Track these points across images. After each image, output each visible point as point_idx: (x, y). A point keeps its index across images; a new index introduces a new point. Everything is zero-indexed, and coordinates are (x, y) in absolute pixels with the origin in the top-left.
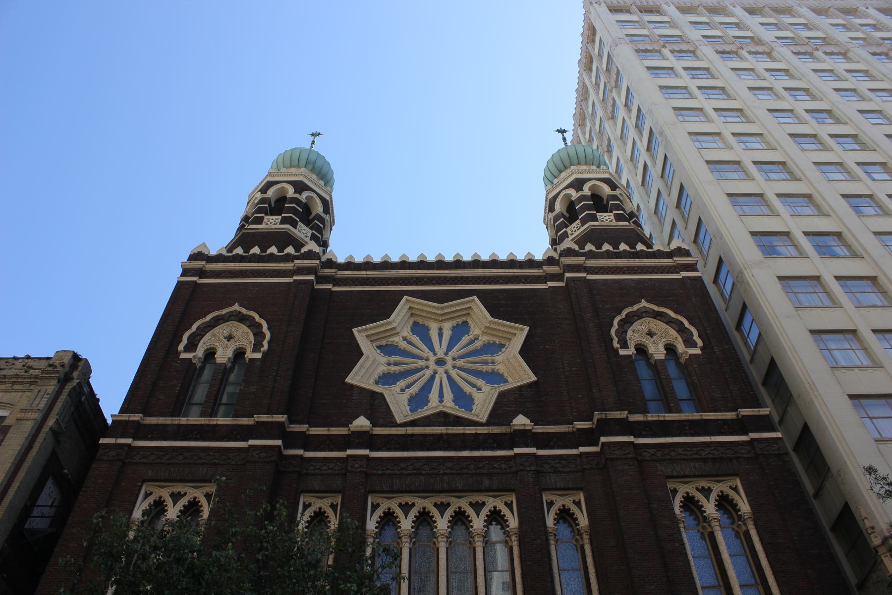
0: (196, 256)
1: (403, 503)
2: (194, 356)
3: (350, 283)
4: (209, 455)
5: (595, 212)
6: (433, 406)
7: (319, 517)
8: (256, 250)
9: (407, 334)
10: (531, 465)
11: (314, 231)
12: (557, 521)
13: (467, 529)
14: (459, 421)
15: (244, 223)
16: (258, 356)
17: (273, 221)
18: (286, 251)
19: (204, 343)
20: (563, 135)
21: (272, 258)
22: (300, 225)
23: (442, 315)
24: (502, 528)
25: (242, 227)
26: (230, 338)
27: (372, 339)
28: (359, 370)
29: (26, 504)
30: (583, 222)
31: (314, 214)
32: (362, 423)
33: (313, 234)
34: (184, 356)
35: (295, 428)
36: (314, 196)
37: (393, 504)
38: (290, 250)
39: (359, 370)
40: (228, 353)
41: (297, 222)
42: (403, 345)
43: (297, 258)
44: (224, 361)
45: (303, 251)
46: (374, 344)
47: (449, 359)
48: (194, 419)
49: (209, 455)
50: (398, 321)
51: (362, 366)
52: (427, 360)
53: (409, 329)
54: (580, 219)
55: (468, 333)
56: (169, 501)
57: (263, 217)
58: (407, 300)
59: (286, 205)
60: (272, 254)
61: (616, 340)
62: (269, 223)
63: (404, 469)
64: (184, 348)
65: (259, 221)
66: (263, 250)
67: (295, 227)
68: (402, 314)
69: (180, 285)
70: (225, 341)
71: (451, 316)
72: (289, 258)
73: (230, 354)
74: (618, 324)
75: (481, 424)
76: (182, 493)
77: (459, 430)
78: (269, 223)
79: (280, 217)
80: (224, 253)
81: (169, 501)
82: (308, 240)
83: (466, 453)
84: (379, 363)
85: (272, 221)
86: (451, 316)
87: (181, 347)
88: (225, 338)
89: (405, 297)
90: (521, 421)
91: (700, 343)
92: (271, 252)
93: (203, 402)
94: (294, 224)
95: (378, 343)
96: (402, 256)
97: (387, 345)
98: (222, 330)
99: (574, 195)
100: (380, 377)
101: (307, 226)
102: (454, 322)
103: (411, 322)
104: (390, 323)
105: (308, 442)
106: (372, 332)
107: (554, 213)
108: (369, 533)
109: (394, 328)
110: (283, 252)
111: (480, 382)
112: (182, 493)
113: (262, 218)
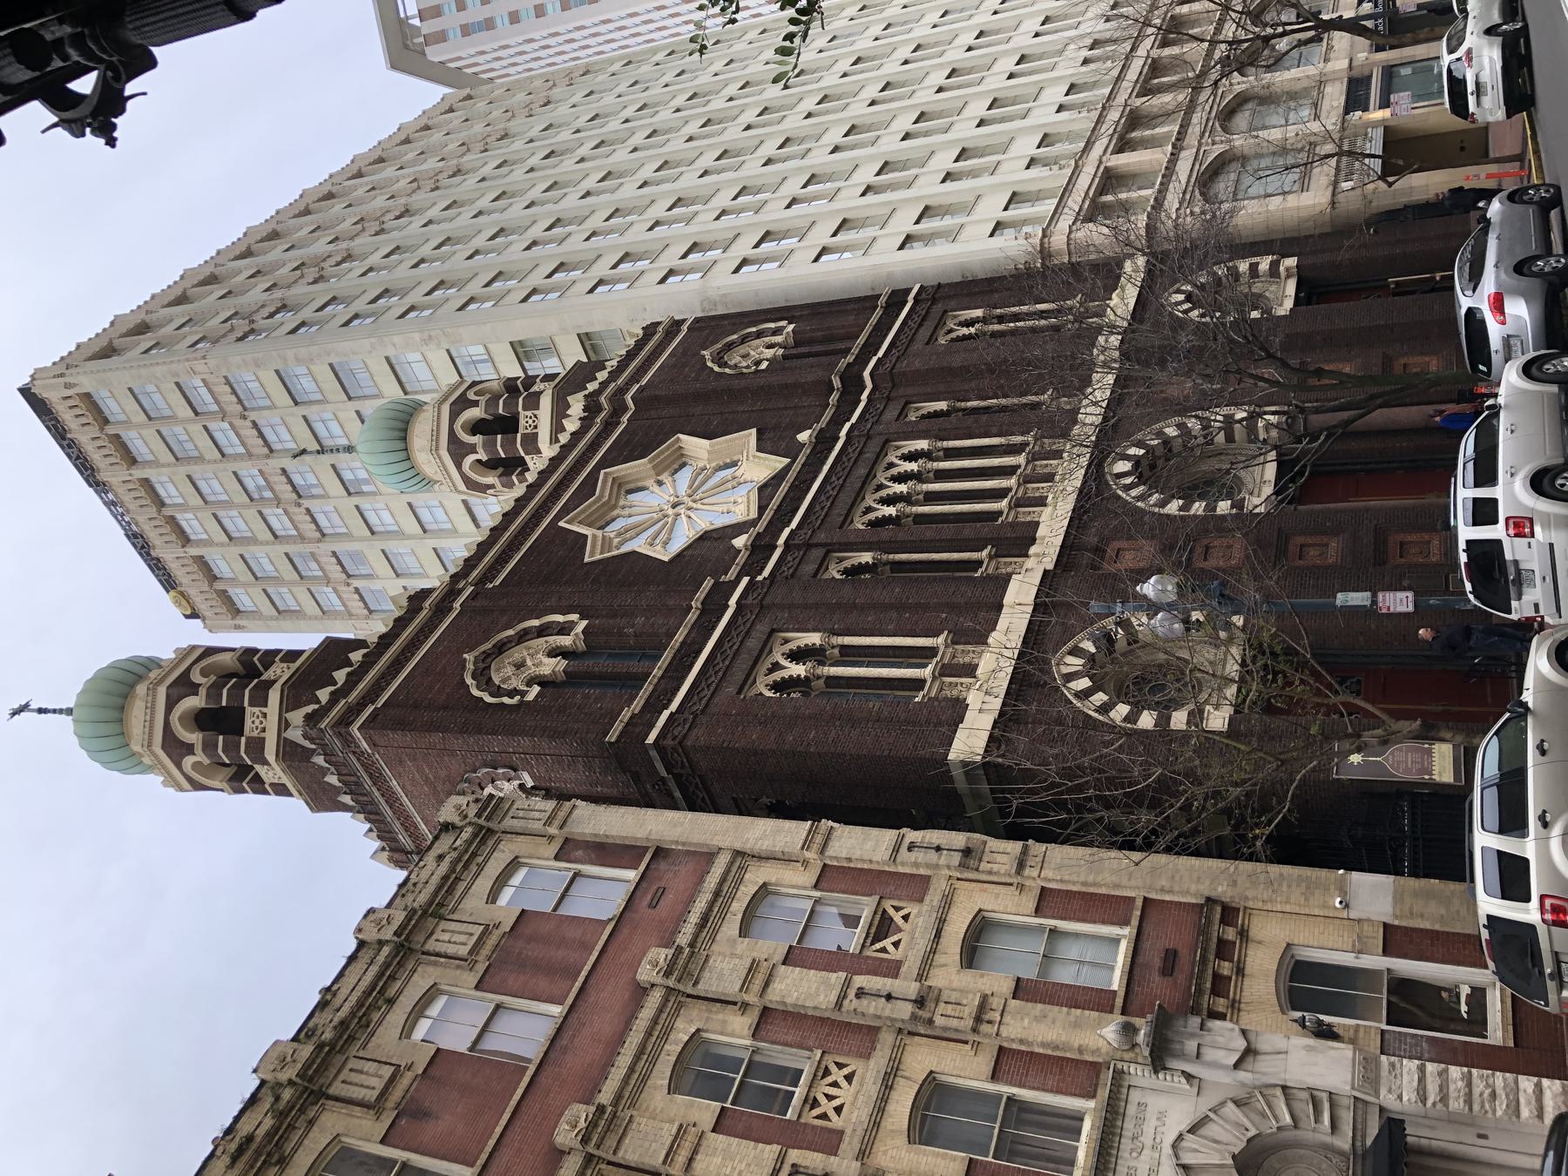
11: (520, 409)
20: (33, 711)
47: (671, 511)
83: (826, 468)
91: (574, 617)
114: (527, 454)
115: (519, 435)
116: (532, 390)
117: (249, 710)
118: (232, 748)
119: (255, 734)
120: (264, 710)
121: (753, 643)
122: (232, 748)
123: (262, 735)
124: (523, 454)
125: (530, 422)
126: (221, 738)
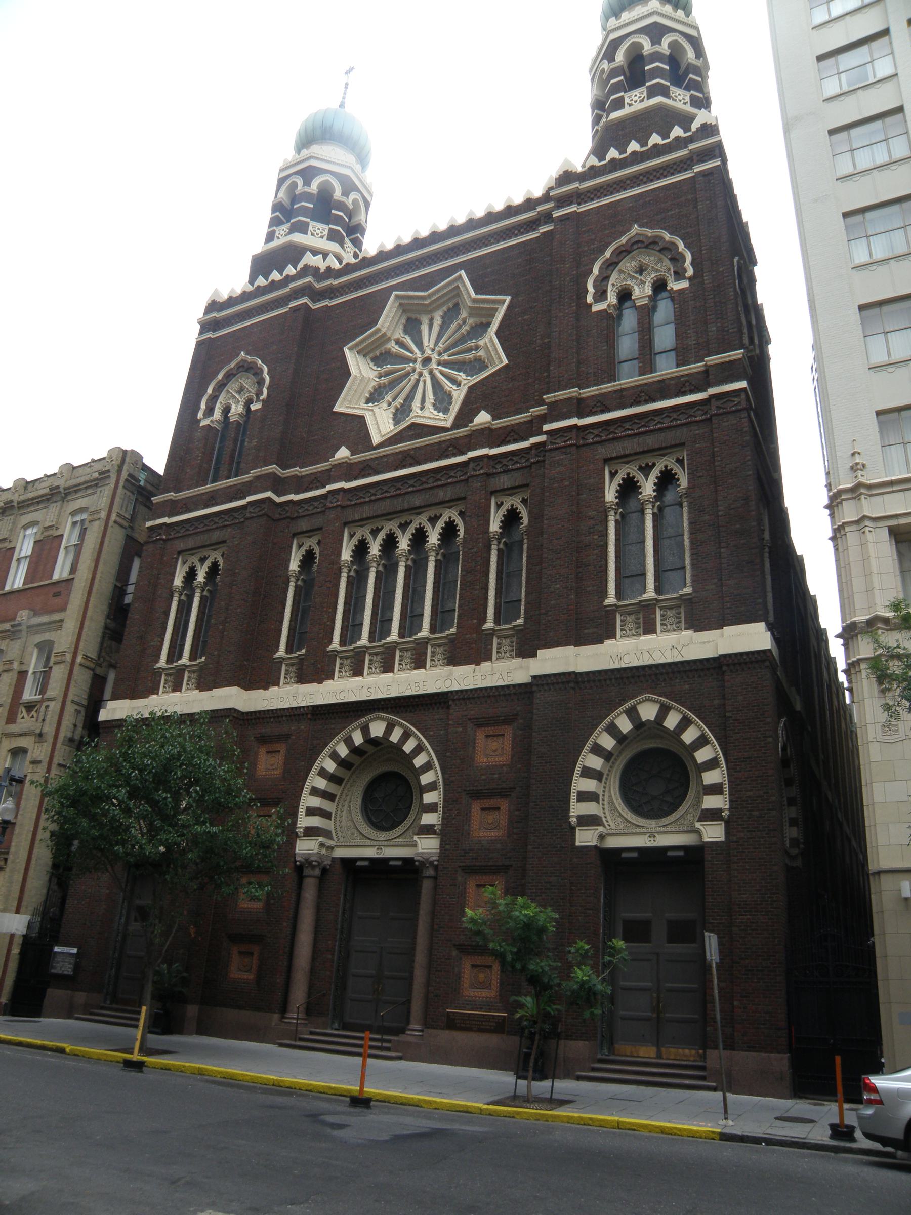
0: (213, 306)
1: (433, 516)
2: (608, 306)
3: (504, 236)
4: (635, 423)
5: (668, 84)
7: (511, 518)
8: (634, 146)
9: (399, 336)
10: (482, 468)
11: (692, 92)
15: (600, 112)
16: (684, 284)
17: (637, 98)
18: (609, 157)
19: (613, 285)
21: (658, 151)
22: (675, 91)
23: (430, 304)
25: (597, 120)
26: (641, 270)
27: (364, 353)
28: (347, 395)
29: (116, 586)
30: (651, 93)
31: (683, 67)
32: (343, 453)
33: (692, 96)
34: (596, 308)
36: (328, 178)
37: (363, 532)
38: (677, 132)
39: (347, 395)
40: (647, 291)
41: (668, 87)
43: (691, 140)
44: (645, 301)
45: (695, 126)
46: (368, 358)
49: (635, 423)
50: (387, 325)
51: (350, 389)
53: (401, 332)
54: (647, 87)
56: (198, 565)
57: (622, 97)
58: (397, 296)
59: (646, 68)
60: (655, 146)
62: (633, 102)
63: (386, 492)
64: (204, 415)
65: (619, 104)
66: (643, 143)
67: (305, 232)
68: (392, 315)
69: (200, 345)
70: (637, 276)
71: (438, 303)
72: (680, 143)
73: (648, 291)
74: (594, 286)
75: (445, 430)
76: (650, 464)
78: (633, 102)
79: (643, 89)
80: (594, 161)
81: (639, 477)
82: (689, 108)
84: (368, 381)
85: (636, 98)
86: (438, 303)
87: (200, 415)
88: (636, 272)
89: (395, 293)
90: (483, 418)
92: (633, 150)
93: (636, 355)
94: (665, 92)
95: (372, 355)
96: (469, 214)
97: (381, 354)
98: (232, 387)
99: (646, 48)
100: (371, 394)
101: (680, 87)
102: (445, 308)
103: (403, 321)
105: (301, 484)
107: (614, 65)
108: (492, 535)
109: (385, 334)
110: (669, 137)
112: (650, 464)
113: (622, 99)
114: (292, 224)
115: (308, 220)
116: (347, 240)
117: (326, 227)
118: (304, 211)
119: (311, 228)
120: (325, 238)
121: (441, 494)
122: (304, 211)
123: (309, 233)
124: (292, 221)
125: (318, 232)
126: (312, 206)
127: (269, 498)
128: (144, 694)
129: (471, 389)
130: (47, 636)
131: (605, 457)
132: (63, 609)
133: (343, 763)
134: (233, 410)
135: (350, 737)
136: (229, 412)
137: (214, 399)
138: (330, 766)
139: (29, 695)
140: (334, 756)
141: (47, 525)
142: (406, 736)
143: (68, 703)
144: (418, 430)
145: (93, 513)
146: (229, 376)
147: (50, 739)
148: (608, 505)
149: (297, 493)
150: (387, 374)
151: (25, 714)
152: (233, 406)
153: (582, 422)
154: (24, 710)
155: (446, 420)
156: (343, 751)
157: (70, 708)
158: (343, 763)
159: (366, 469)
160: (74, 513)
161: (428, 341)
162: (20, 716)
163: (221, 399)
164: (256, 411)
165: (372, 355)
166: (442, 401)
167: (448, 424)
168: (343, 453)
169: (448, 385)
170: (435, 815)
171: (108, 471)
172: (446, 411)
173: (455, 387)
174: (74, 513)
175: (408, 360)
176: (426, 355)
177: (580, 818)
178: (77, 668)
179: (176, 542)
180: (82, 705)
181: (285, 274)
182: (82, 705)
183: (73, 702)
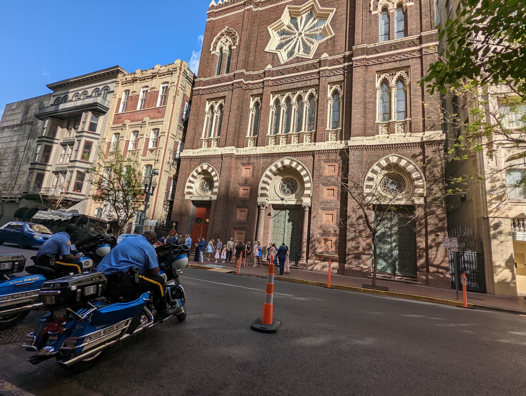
6: (295, 55)
12: (397, 82)
13: (387, 85)
14: (303, 60)
24: (387, 85)
34: (212, 53)
35: (248, 73)
42: (287, 29)
48: (216, 77)
52: (305, 35)
55: (482, 23)
61: (372, 6)
75: (310, 59)
77: (305, 63)
87: (211, 50)
89: (287, 6)
98: (223, 39)
104: (281, 20)
106: (274, 27)
111: (284, 41)
121: (309, 83)
127: (242, 81)
128: (197, 148)
129: (320, 45)
130: (156, 127)
131: (377, 70)
132: (163, 116)
133: (279, 170)
134: (224, 49)
135: (283, 161)
136: (222, 49)
137: (216, 43)
138: (274, 169)
139: (151, 146)
140: (276, 166)
141: (152, 87)
142: (213, 170)
143: (167, 150)
144: (299, 59)
145: (171, 83)
146: (222, 35)
147: (161, 162)
148: (377, 88)
149: (252, 81)
150: (284, 39)
151: (150, 153)
152: (224, 47)
153: (367, 57)
154: (149, 152)
155: (311, 56)
156: (280, 165)
157: (168, 152)
158: (279, 170)
159: (281, 73)
160: (144, 87)
161: (300, 28)
162: (148, 154)
163: (219, 43)
164: (234, 49)
165: (277, 31)
166: (307, 49)
167: (311, 58)
168: (269, 67)
169: (309, 44)
170: (310, 184)
171: (177, 68)
172: (308, 53)
173: (311, 44)
174: (144, 87)
175: (293, 34)
176: (299, 32)
177: (261, 194)
178: (169, 138)
179: (205, 95)
180: (172, 151)
181: (218, 3)
182: (172, 151)
183: (169, 149)
